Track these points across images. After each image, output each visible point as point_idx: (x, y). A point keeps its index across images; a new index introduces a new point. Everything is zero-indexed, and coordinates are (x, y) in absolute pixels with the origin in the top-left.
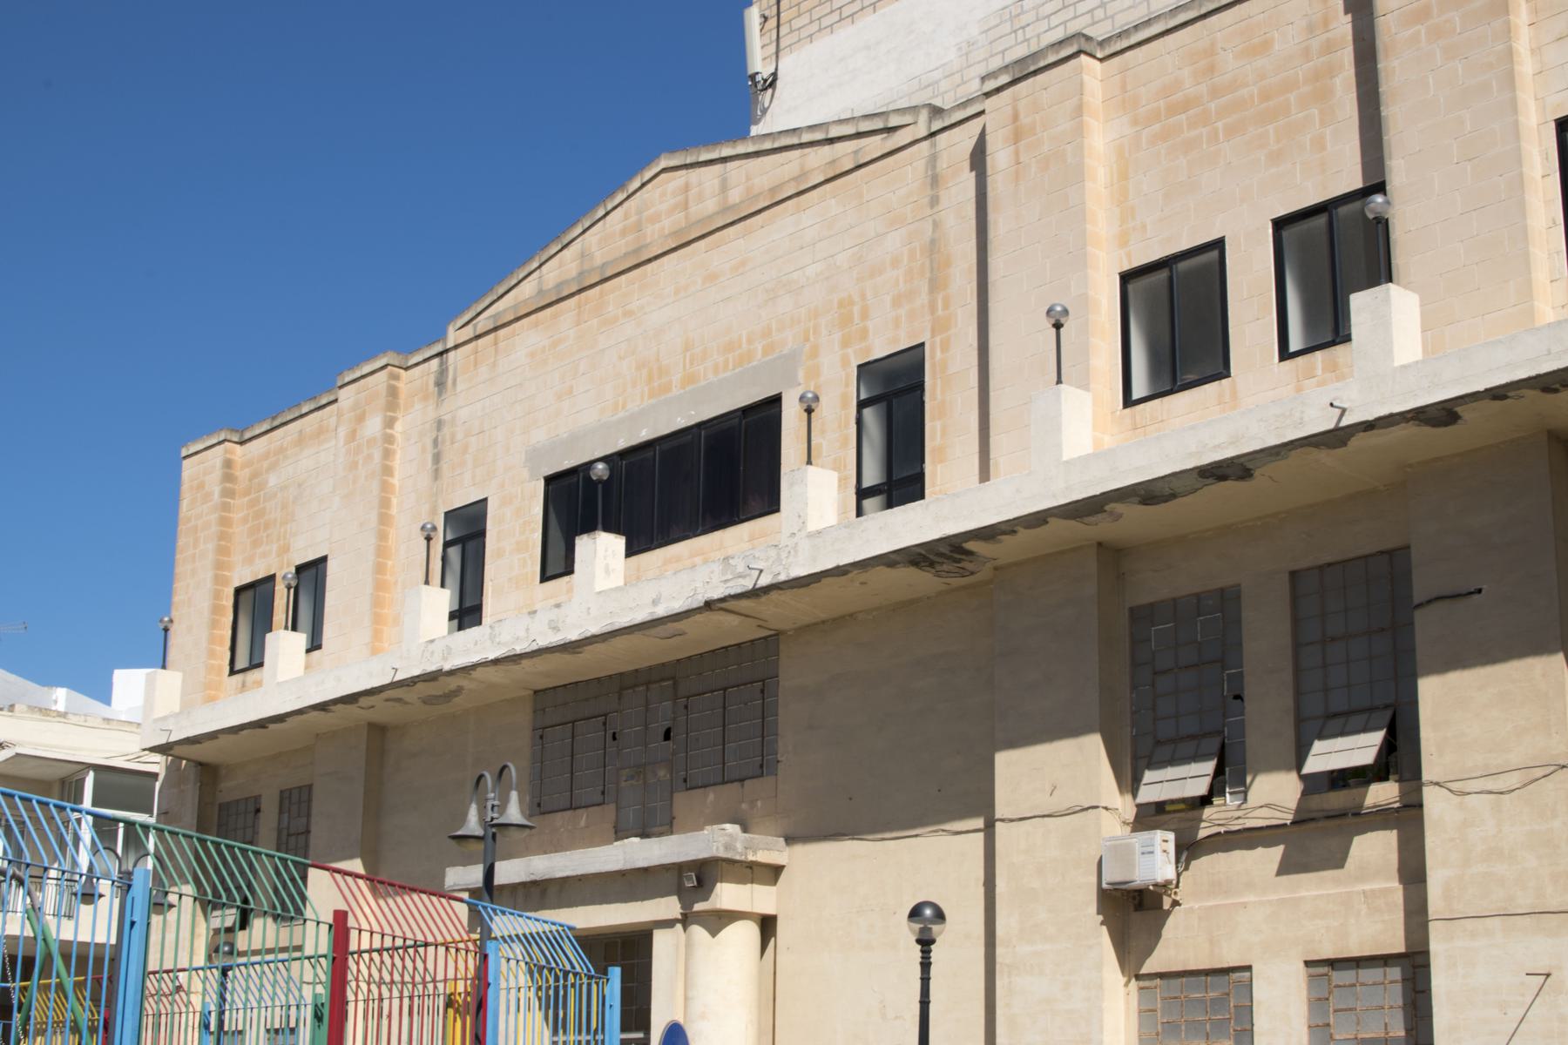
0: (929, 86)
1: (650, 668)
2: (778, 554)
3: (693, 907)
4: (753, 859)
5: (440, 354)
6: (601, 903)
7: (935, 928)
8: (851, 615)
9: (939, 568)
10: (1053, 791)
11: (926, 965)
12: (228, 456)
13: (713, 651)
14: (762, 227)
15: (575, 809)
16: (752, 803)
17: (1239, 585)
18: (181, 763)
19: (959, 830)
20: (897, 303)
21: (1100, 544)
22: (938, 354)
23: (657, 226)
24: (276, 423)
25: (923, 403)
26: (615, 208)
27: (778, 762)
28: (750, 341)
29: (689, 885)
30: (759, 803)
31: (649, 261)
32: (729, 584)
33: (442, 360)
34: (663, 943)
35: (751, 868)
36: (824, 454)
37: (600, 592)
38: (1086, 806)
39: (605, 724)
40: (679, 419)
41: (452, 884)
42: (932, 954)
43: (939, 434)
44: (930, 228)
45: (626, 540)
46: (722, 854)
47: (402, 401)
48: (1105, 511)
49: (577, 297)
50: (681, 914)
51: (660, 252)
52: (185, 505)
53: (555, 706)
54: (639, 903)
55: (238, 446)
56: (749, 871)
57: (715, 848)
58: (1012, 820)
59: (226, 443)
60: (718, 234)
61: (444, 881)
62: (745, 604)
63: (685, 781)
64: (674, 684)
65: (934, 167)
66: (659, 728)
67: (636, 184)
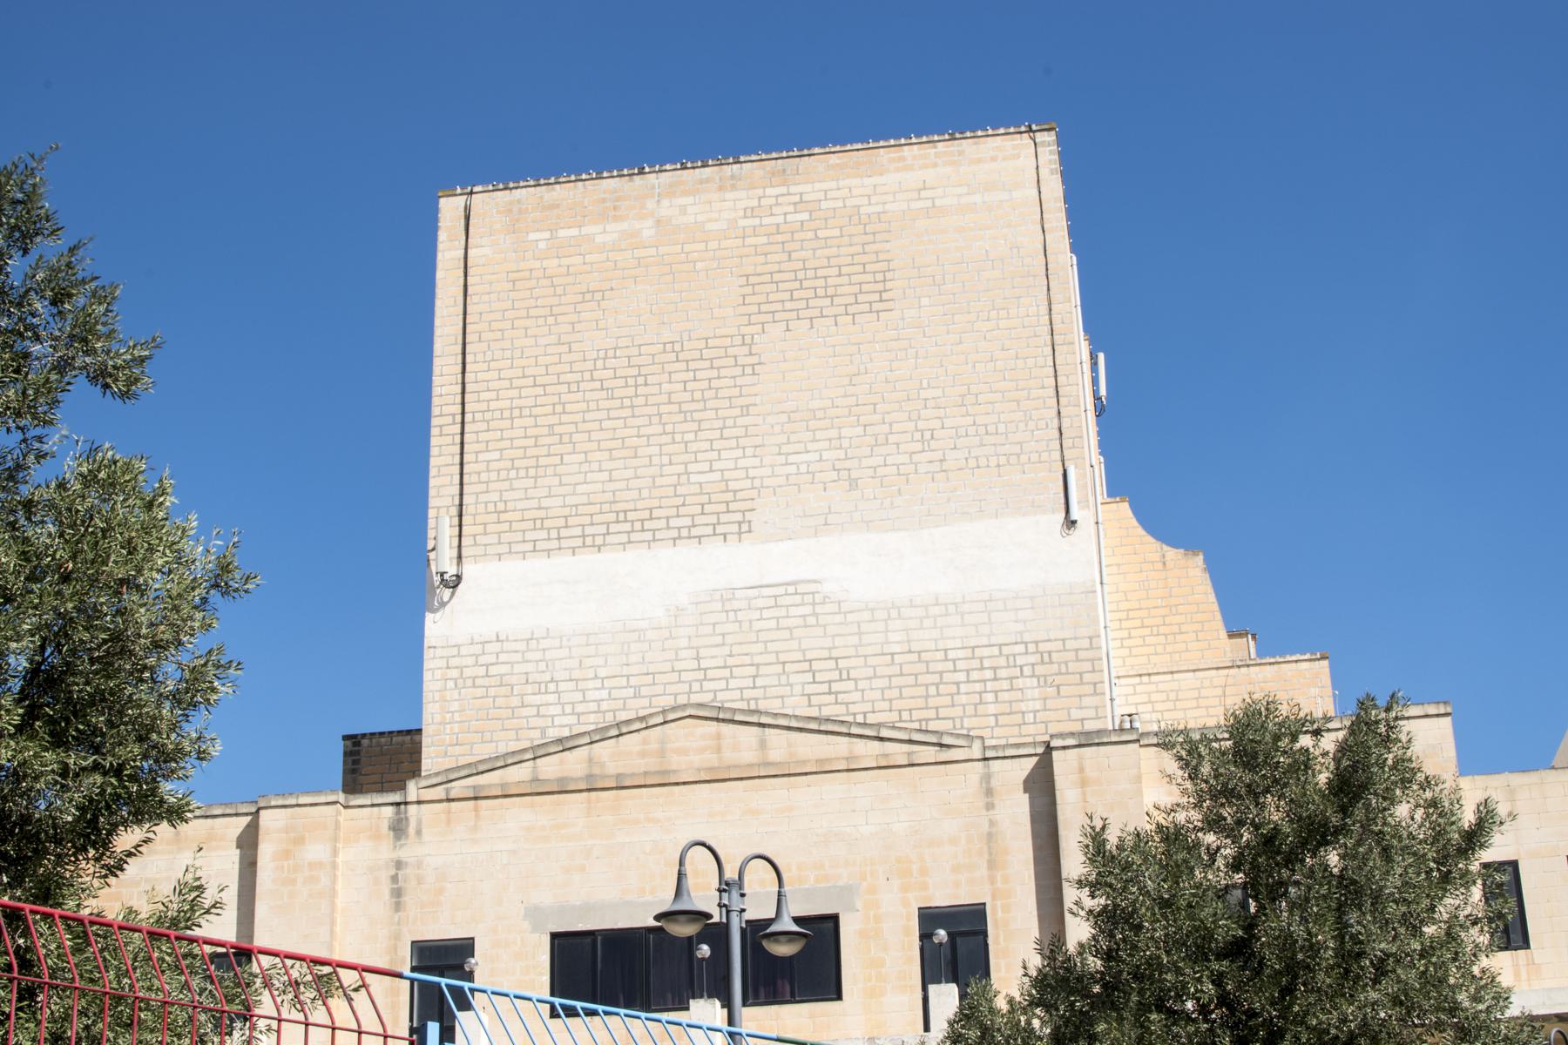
0: (634, 631)
5: (398, 804)
17: (473, 939)
22: (1000, 914)
25: (986, 945)
44: (987, 826)
60: (757, 780)
65: (988, 782)
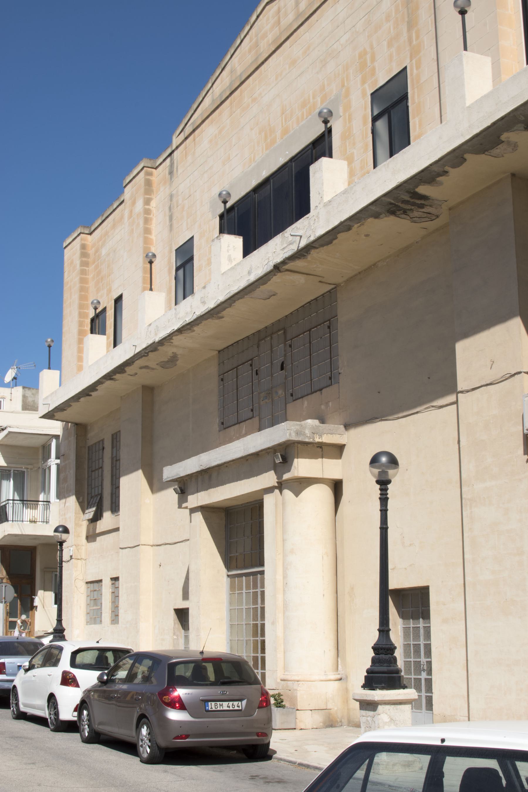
1: (273, 324)
2: (309, 223)
3: (282, 477)
4: (320, 440)
5: (170, 154)
6: (237, 481)
7: (391, 472)
8: (374, 265)
9: (411, 215)
10: (492, 365)
11: (384, 500)
12: (83, 242)
13: (303, 306)
14: (317, 21)
15: (239, 423)
16: (327, 404)
18: (69, 424)
19: (442, 405)
20: (390, 45)
21: (513, 175)
22: (415, 71)
23: (266, 40)
24: (104, 218)
26: (245, 36)
27: (340, 373)
28: (314, 98)
29: (277, 461)
30: (330, 404)
31: (263, 63)
32: (285, 250)
33: (171, 158)
34: (269, 501)
35: (321, 447)
36: (355, 159)
37: (223, 273)
38: (513, 373)
39: (251, 365)
40: (281, 159)
41: (166, 477)
42: (388, 492)
43: (417, 126)
45: (243, 239)
46: (294, 438)
47: (154, 188)
48: (503, 142)
49: (230, 98)
50: (277, 482)
51: (267, 55)
52: (66, 275)
53: (228, 359)
54: (255, 477)
55: (89, 236)
56: (319, 450)
57: (288, 434)
58: (468, 391)
59: (81, 235)
61: (162, 476)
62: (299, 264)
63: (292, 395)
64: (284, 332)
66: (277, 363)
67: (254, 17)
